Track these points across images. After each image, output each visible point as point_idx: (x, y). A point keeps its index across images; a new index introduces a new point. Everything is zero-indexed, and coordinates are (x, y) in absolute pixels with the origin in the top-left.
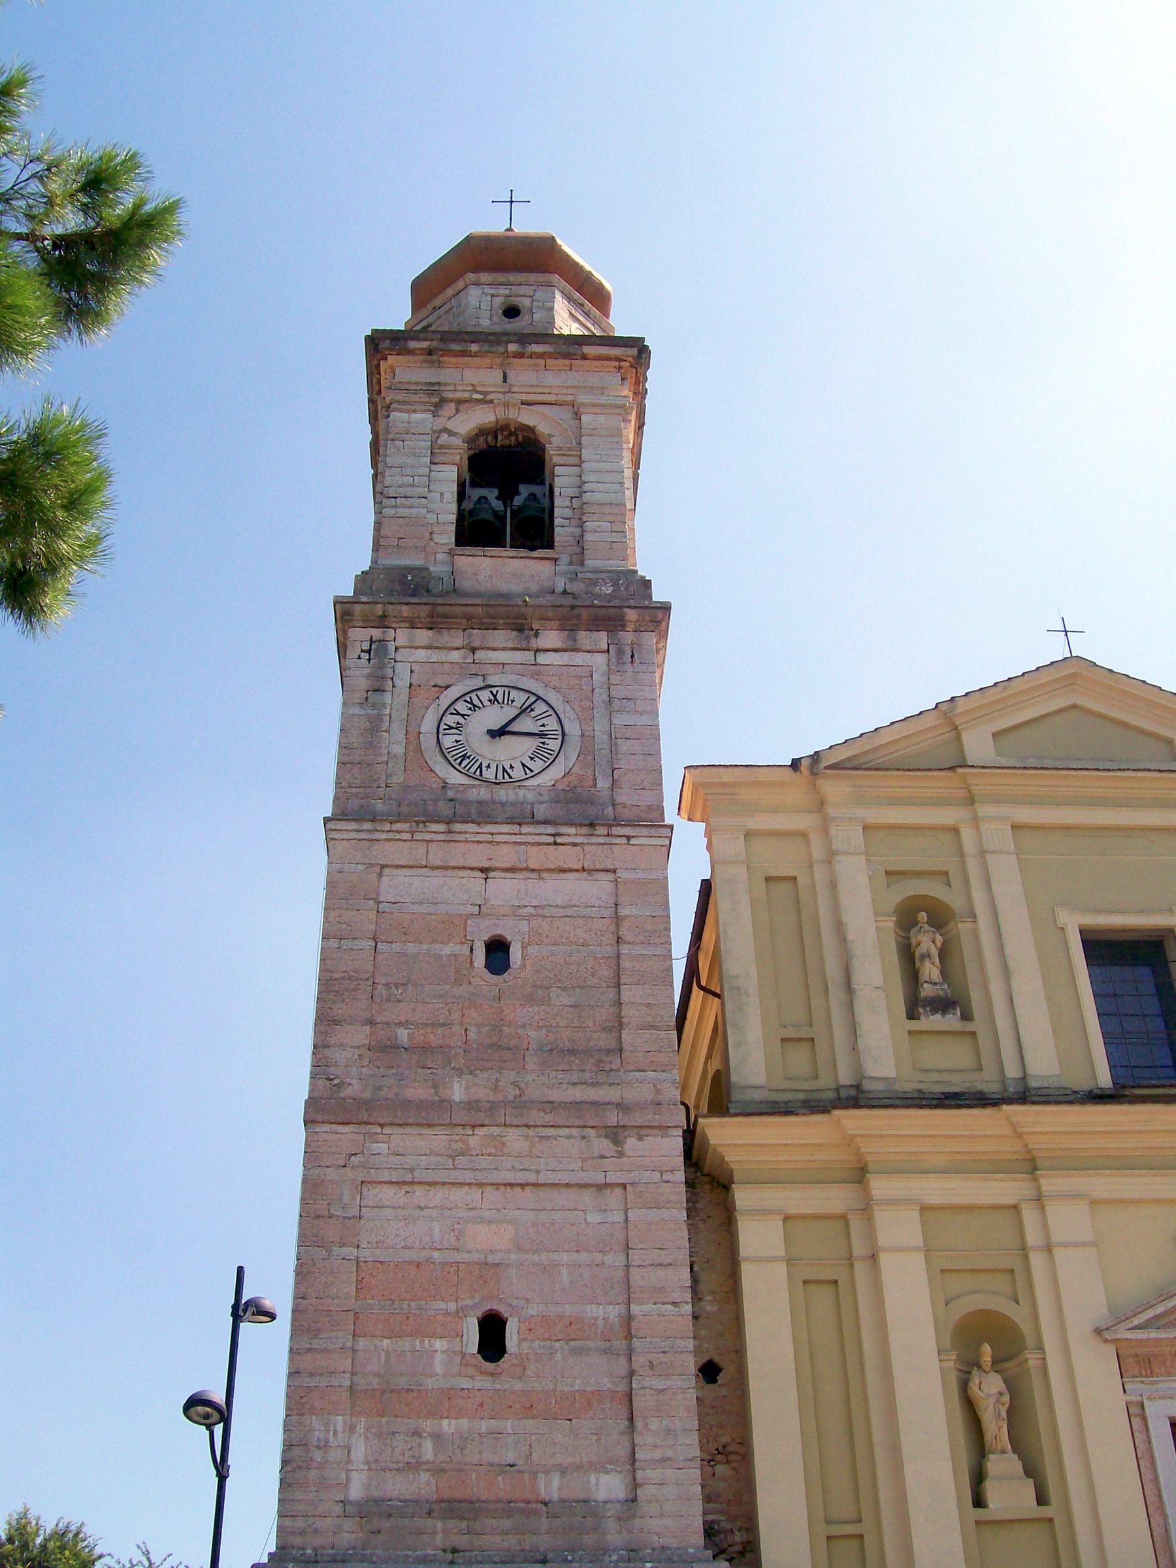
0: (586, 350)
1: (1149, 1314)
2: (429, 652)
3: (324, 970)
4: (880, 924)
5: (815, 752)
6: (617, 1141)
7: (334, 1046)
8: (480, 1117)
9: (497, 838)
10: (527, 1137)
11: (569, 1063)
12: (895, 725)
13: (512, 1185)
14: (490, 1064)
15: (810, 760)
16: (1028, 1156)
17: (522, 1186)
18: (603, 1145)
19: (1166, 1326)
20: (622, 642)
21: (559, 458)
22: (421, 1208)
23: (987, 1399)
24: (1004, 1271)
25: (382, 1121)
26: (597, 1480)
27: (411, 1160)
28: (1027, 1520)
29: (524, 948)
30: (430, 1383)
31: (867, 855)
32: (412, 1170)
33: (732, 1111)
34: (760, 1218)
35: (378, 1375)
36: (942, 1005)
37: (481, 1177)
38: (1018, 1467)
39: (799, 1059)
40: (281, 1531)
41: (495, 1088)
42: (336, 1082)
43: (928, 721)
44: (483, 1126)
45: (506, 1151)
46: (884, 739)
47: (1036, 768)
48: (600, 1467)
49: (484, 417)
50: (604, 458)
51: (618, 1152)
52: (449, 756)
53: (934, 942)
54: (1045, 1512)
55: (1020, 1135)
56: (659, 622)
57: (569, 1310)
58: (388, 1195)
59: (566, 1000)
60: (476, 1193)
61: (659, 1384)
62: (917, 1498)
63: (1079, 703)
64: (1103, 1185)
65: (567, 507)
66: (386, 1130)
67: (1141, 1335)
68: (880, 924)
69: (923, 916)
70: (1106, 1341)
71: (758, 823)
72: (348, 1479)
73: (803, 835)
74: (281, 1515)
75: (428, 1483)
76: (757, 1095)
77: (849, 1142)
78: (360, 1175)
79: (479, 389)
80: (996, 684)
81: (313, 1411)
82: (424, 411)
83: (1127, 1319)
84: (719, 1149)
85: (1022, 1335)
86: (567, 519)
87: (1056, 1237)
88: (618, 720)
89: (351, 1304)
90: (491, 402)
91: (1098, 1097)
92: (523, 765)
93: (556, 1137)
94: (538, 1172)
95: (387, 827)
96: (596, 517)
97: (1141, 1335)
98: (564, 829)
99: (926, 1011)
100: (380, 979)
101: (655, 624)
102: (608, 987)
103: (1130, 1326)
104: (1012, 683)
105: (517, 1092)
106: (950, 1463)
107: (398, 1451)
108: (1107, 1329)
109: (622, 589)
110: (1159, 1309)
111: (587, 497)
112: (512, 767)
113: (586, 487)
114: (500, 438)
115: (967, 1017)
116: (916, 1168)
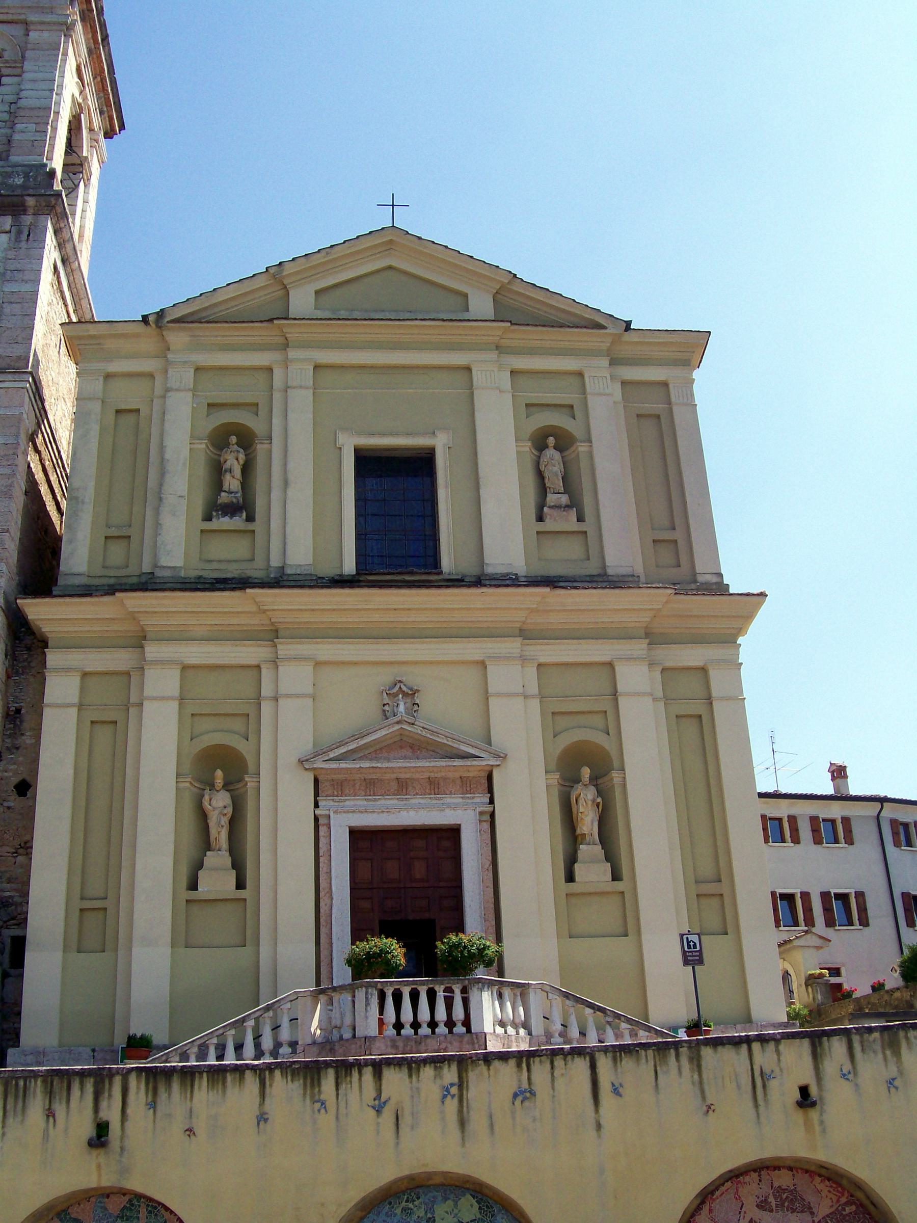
4: (193, 446)
5: (161, 310)
12: (231, 285)
15: (155, 316)
16: (273, 628)
19: (361, 758)
20: (22, 224)
23: (214, 811)
24: (600, 712)
28: (226, 900)
33: (54, 593)
34: (63, 674)
36: (231, 510)
38: (228, 861)
39: (117, 552)
43: (261, 282)
46: (219, 297)
47: (365, 320)
50: (41, 69)
53: (237, 459)
54: (242, 894)
56: (54, 207)
62: (143, 882)
64: (326, 650)
65: (5, 112)
67: (334, 765)
68: (193, 446)
69: (234, 439)
70: (306, 769)
71: (115, 367)
73: (151, 376)
76: (77, 581)
77: (133, 617)
80: (319, 251)
83: (324, 753)
84: (38, 623)
85: (246, 765)
86: (4, 122)
87: (282, 690)
91: (341, 582)
96: (25, 120)
97: (334, 765)
99: (218, 515)
101: (50, 208)
103: (327, 758)
104: (336, 249)
106: (172, 858)
108: (307, 760)
109: (31, 180)
110: (352, 746)
116: (182, 636)
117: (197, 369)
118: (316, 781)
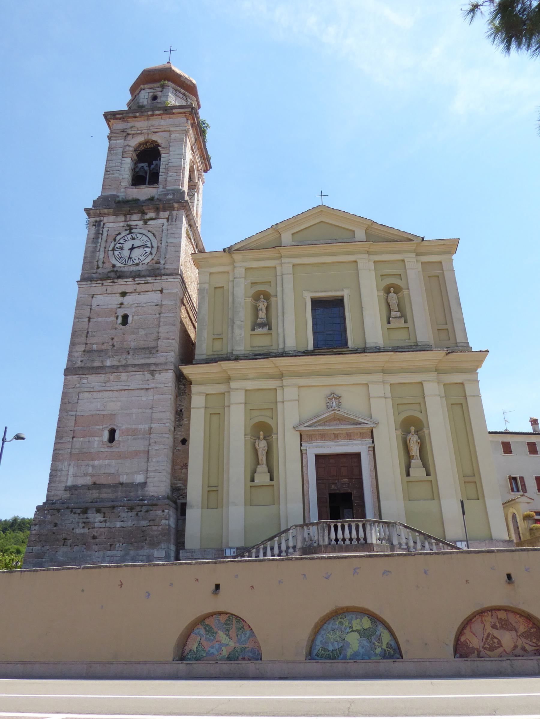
0: (174, 111)
1: (311, 422)
2: (114, 223)
3: (73, 328)
6: (153, 375)
7: (74, 352)
8: (114, 370)
9: (128, 283)
10: (127, 375)
11: (142, 352)
13: (121, 390)
14: (118, 354)
15: (228, 249)
16: (281, 373)
17: (125, 390)
18: (148, 376)
19: (318, 426)
21: (163, 151)
22: (95, 399)
25: (86, 374)
26: (137, 476)
27: (93, 385)
29: (133, 317)
30: (93, 450)
31: (245, 278)
32: (93, 388)
33: (194, 363)
35: (78, 449)
36: (262, 325)
37: (112, 388)
40: (48, 496)
41: (119, 362)
42: (74, 362)
44: (115, 373)
45: (120, 380)
48: (137, 473)
49: (141, 139)
51: (153, 378)
52: (116, 258)
53: (264, 305)
54: (272, 483)
55: (277, 367)
57: (134, 426)
58: (86, 395)
59: (144, 332)
60: (111, 393)
61: (157, 448)
63: (324, 220)
64: (302, 381)
66: (87, 376)
67: (308, 429)
69: (262, 297)
70: (297, 431)
72: (67, 480)
74: (48, 491)
75: (90, 480)
77: (225, 371)
78: (78, 390)
79: (139, 129)
80: (292, 217)
81: (59, 460)
82: (121, 139)
88: (170, 241)
89: (72, 428)
90: (143, 133)
91: (311, 353)
92: (139, 258)
93: (135, 375)
94: (129, 386)
95: (95, 282)
97: (308, 429)
98: (148, 278)
100: (90, 330)
102: (156, 327)
105: (126, 362)
107: (82, 471)
110: (315, 421)
111: (170, 165)
112: (135, 259)
113: (170, 161)
114: (148, 145)
115: (270, 329)
116: (244, 378)
117: (246, 269)
118: (301, 435)
